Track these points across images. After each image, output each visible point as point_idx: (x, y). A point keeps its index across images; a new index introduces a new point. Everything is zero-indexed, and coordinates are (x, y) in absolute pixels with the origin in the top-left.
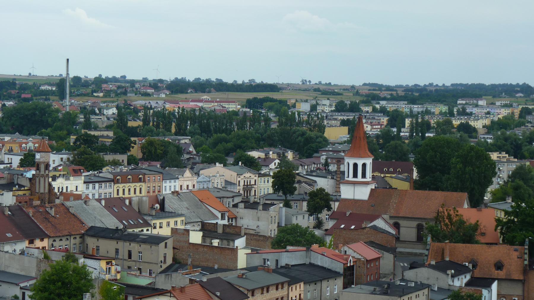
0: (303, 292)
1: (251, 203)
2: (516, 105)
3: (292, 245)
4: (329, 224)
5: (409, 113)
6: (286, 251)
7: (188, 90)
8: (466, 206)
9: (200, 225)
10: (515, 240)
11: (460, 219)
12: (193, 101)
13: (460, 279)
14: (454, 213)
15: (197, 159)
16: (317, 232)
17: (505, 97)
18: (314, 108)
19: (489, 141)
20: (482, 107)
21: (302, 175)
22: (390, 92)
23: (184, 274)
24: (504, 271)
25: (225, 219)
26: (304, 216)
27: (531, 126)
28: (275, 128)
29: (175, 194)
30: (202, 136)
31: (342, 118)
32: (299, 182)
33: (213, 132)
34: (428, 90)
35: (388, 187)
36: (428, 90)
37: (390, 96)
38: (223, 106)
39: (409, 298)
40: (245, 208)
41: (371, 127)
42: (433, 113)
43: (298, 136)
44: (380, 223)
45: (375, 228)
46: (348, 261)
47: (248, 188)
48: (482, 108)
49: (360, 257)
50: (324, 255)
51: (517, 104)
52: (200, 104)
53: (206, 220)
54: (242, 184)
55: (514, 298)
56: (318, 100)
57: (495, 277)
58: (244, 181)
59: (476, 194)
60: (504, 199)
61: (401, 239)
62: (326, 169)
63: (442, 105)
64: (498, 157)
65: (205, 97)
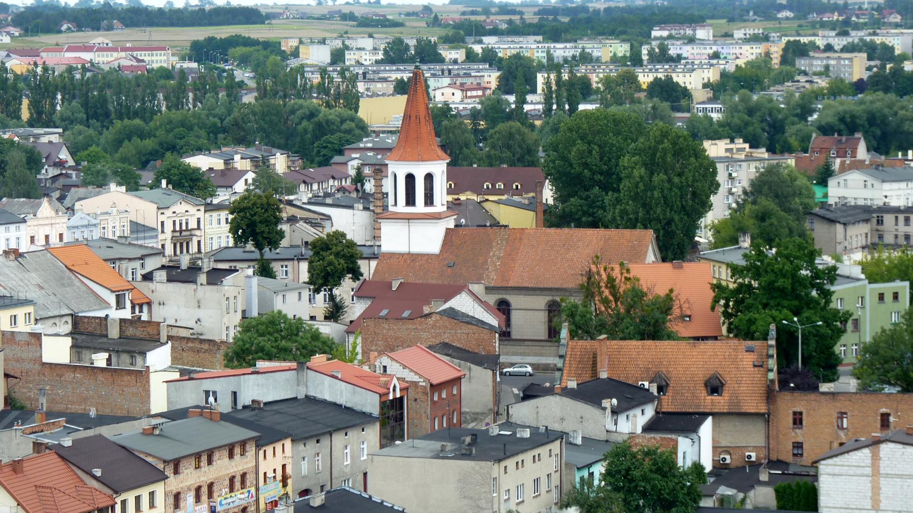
0: (290, 460)
1: (182, 270)
2: (778, 37)
3: (270, 357)
4: (356, 310)
5: (545, 61)
6: (253, 373)
7: (62, 26)
8: (651, 257)
9: (70, 322)
10: (753, 328)
11: (633, 289)
12: (71, 49)
13: (630, 418)
14: (622, 274)
15: (74, 176)
16: (327, 329)
17: (754, 21)
18: (338, 56)
19: (715, 116)
20: (702, 42)
21: (299, 203)
22: (507, 17)
23: (28, 431)
24: (726, 395)
25: (124, 308)
26: (300, 293)
27: (807, 81)
28: (250, 103)
29: (12, 257)
30: (88, 127)
31: (398, 76)
32: (292, 220)
33: (113, 116)
34: (591, 10)
35: (488, 224)
36: (591, 10)
37: (506, 26)
38: (139, 57)
39: (517, 463)
40: (170, 280)
41: (463, 93)
42: (598, 60)
43: (302, 119)
44: (463, 303)
45: (452, 314)
46: (389, 389)
47: (182, 238)
48: (703, 44)
49: (416, 378)
50: (336, 378)
51: (778, 34)
52: (87, 56)
53: (83, 312)
54: (169, 227)
56: (349, 38)
57: (705, 410)
58: (174, 222)
59: (677, 231)
60: (734, 241)
61: (515, 335)
62: (357, 190)
63: (618, 41)
64: (727, 150)
65: (99, 38)
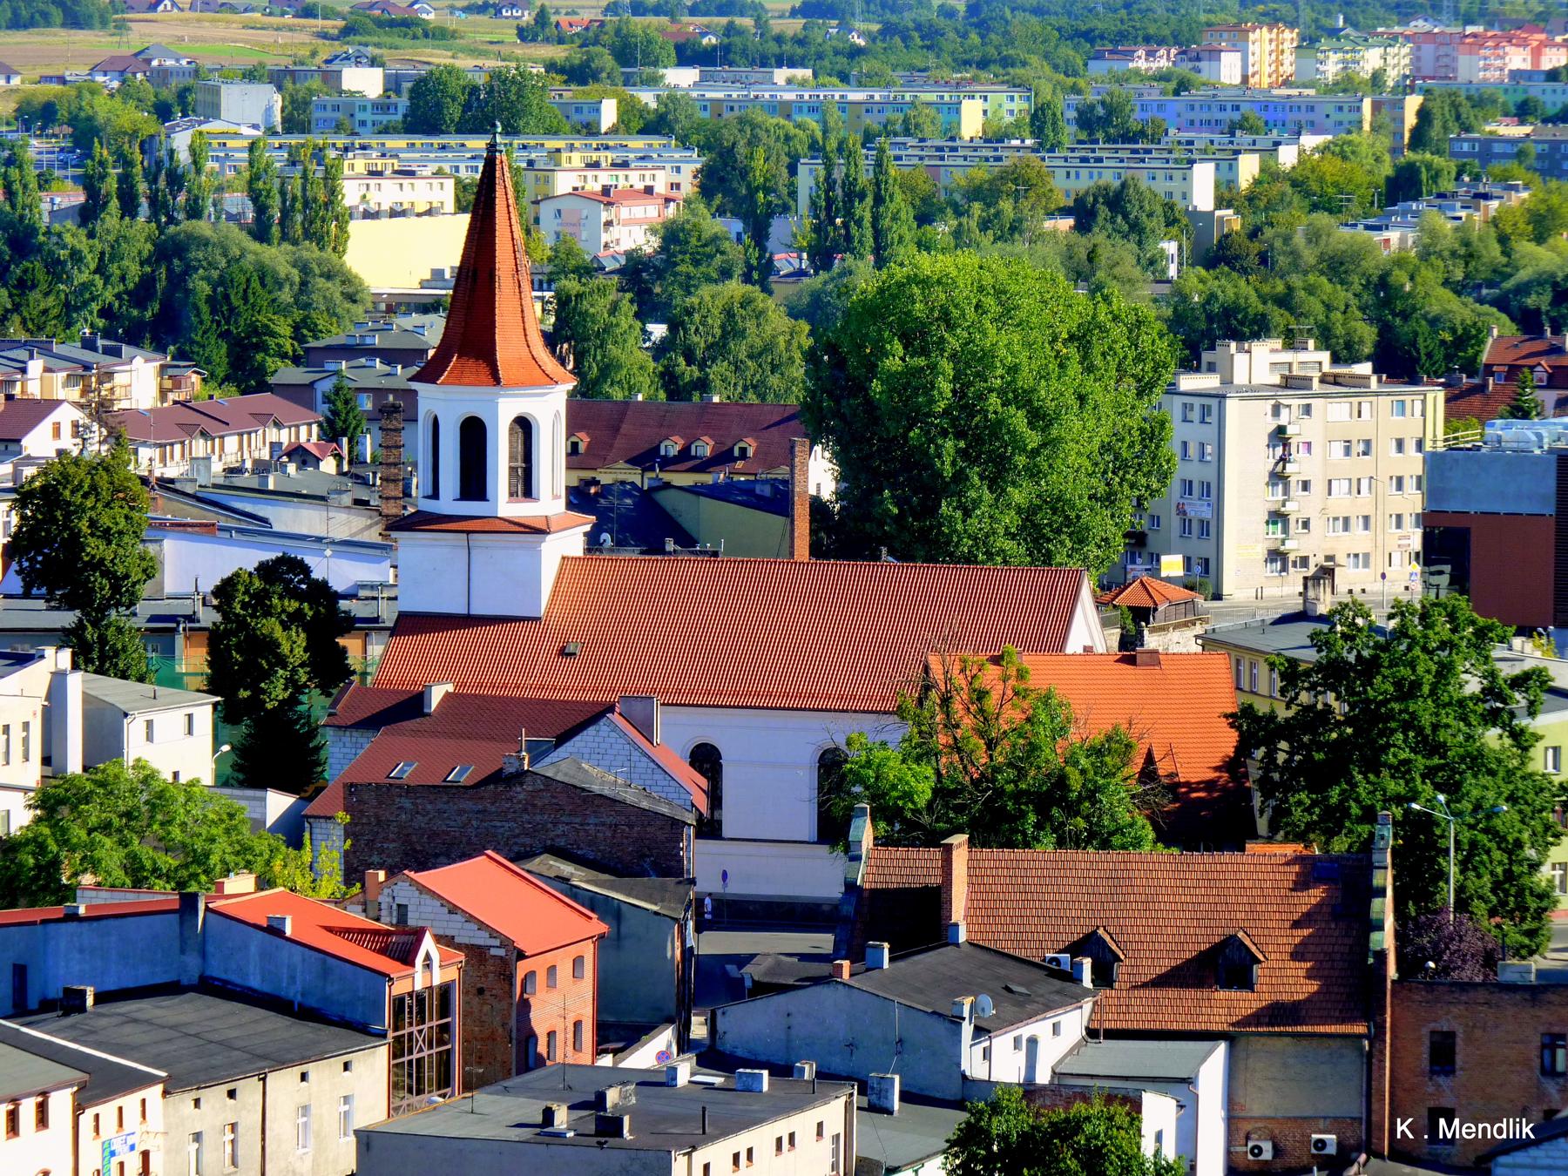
55: (1315, 1136)
